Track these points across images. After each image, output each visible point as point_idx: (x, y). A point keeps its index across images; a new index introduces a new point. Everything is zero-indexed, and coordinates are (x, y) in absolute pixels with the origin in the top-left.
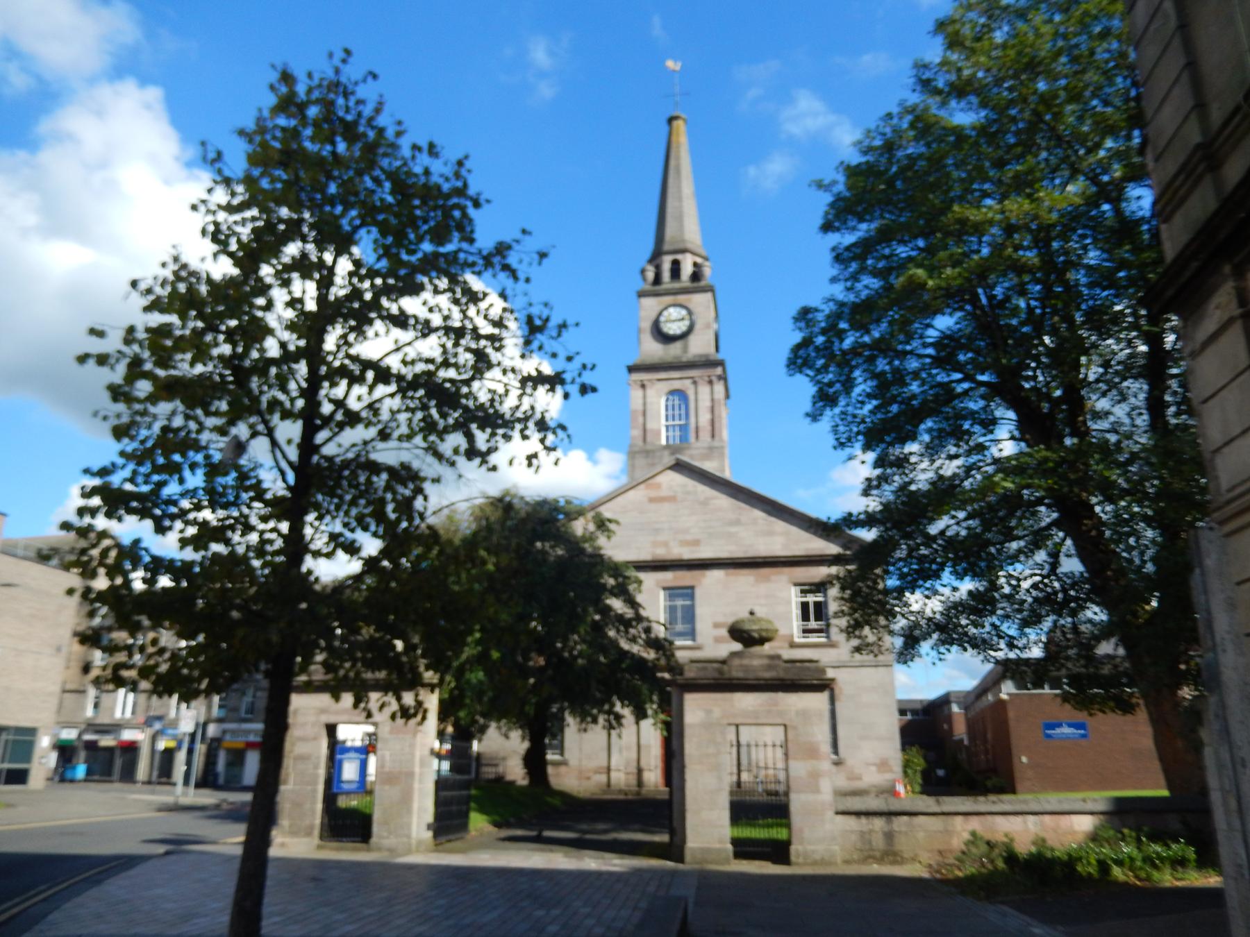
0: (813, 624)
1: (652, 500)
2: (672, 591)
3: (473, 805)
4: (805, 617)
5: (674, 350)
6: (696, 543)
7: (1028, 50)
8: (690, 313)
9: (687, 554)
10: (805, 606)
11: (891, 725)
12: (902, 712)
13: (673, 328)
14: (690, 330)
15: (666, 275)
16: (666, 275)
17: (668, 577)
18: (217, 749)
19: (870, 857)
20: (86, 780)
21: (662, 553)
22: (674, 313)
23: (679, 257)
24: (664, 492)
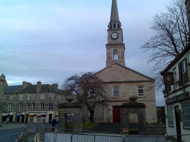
0: (141, 93)
1: (111, 70)
2: (115, 88)
3: (176, 137)
4: (139, 92)
5: (115, 41)
6: (119, 78)
7: (180, 3)
8: (117, 34)
9: (117, 81)
10: (139, 90)
11: (155, 111)
12: (157, 108)
13: (115, 37)
14: (118, 37)
15: (113, 26)
16: (113, 26)
17: (114, 85)
18: (28, 116)
19: (181, 7)
20: (15, 122)
21: (113, 80)
22: (115, 34)
23: (115, 23)
24: (113, 69)
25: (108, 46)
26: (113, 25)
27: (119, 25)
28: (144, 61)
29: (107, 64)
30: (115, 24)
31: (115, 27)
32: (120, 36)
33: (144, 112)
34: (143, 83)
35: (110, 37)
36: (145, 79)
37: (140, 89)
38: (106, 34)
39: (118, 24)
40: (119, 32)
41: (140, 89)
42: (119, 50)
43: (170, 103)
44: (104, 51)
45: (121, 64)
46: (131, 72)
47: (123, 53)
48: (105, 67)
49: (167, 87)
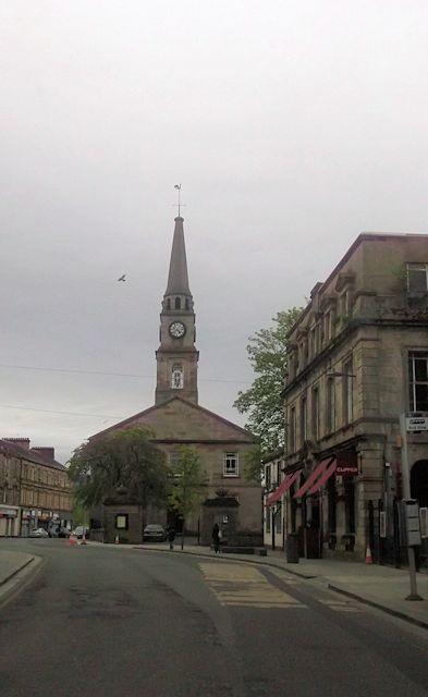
0: (230, 469)
6: (184, 433)
9: (180, 438)
16: (173, 306)
22: (179, 326)
25: (162, 353)
26: (173, 302)
27: (189, 297)
28: (225, 387)
29: (156, 402)
30: (178, 300)
31: (178, 306)
32: (189, 332)
33: (237, 513)
34: (238, 446)
35: (166, 332)
36: (242, 438)
37: (231, 459)
38: (155, 322)
39: (187, 300)
40: (188, 320)
41: (231, 459)
42: (186, 365)
43: (316, 366)
44: (151, 365)
45: (191, 400)
46: (212, 420)
47: (194, 373)
48: (153, 404)
49: (347, 392)
